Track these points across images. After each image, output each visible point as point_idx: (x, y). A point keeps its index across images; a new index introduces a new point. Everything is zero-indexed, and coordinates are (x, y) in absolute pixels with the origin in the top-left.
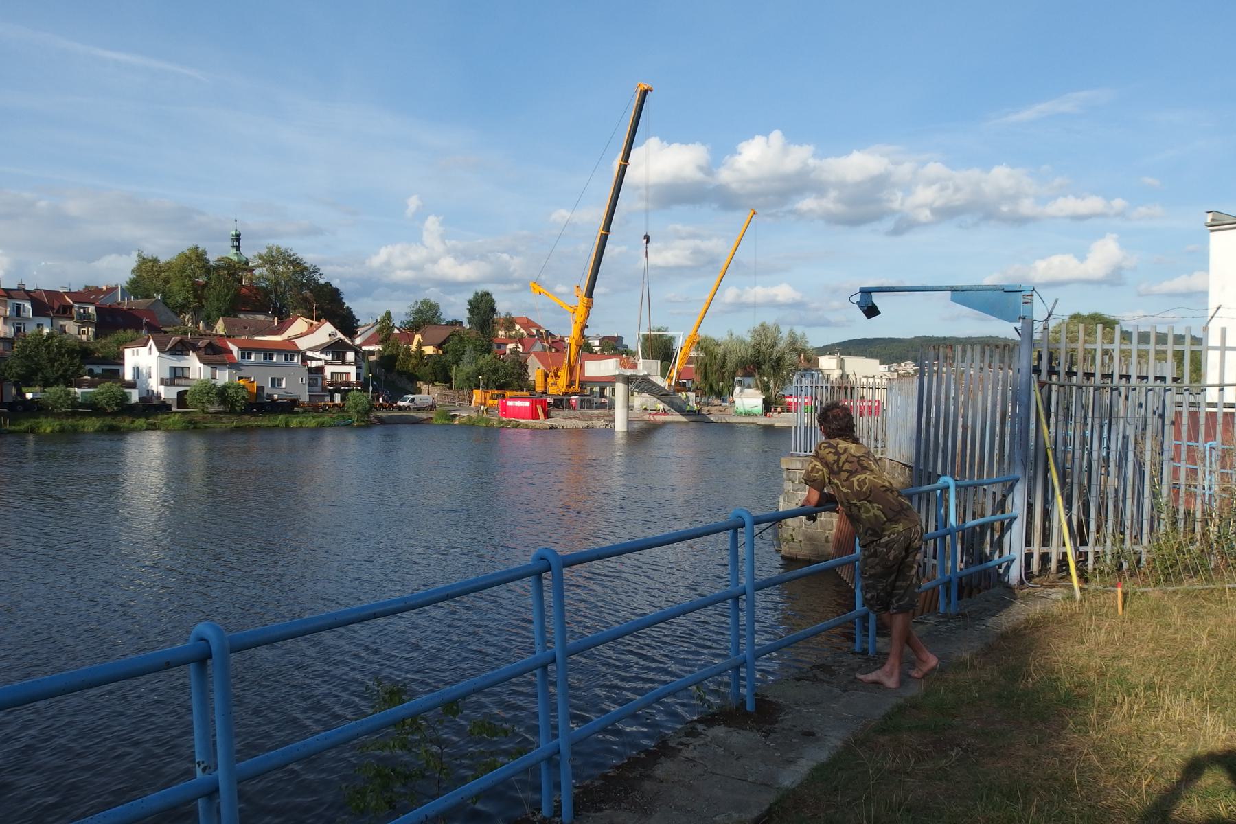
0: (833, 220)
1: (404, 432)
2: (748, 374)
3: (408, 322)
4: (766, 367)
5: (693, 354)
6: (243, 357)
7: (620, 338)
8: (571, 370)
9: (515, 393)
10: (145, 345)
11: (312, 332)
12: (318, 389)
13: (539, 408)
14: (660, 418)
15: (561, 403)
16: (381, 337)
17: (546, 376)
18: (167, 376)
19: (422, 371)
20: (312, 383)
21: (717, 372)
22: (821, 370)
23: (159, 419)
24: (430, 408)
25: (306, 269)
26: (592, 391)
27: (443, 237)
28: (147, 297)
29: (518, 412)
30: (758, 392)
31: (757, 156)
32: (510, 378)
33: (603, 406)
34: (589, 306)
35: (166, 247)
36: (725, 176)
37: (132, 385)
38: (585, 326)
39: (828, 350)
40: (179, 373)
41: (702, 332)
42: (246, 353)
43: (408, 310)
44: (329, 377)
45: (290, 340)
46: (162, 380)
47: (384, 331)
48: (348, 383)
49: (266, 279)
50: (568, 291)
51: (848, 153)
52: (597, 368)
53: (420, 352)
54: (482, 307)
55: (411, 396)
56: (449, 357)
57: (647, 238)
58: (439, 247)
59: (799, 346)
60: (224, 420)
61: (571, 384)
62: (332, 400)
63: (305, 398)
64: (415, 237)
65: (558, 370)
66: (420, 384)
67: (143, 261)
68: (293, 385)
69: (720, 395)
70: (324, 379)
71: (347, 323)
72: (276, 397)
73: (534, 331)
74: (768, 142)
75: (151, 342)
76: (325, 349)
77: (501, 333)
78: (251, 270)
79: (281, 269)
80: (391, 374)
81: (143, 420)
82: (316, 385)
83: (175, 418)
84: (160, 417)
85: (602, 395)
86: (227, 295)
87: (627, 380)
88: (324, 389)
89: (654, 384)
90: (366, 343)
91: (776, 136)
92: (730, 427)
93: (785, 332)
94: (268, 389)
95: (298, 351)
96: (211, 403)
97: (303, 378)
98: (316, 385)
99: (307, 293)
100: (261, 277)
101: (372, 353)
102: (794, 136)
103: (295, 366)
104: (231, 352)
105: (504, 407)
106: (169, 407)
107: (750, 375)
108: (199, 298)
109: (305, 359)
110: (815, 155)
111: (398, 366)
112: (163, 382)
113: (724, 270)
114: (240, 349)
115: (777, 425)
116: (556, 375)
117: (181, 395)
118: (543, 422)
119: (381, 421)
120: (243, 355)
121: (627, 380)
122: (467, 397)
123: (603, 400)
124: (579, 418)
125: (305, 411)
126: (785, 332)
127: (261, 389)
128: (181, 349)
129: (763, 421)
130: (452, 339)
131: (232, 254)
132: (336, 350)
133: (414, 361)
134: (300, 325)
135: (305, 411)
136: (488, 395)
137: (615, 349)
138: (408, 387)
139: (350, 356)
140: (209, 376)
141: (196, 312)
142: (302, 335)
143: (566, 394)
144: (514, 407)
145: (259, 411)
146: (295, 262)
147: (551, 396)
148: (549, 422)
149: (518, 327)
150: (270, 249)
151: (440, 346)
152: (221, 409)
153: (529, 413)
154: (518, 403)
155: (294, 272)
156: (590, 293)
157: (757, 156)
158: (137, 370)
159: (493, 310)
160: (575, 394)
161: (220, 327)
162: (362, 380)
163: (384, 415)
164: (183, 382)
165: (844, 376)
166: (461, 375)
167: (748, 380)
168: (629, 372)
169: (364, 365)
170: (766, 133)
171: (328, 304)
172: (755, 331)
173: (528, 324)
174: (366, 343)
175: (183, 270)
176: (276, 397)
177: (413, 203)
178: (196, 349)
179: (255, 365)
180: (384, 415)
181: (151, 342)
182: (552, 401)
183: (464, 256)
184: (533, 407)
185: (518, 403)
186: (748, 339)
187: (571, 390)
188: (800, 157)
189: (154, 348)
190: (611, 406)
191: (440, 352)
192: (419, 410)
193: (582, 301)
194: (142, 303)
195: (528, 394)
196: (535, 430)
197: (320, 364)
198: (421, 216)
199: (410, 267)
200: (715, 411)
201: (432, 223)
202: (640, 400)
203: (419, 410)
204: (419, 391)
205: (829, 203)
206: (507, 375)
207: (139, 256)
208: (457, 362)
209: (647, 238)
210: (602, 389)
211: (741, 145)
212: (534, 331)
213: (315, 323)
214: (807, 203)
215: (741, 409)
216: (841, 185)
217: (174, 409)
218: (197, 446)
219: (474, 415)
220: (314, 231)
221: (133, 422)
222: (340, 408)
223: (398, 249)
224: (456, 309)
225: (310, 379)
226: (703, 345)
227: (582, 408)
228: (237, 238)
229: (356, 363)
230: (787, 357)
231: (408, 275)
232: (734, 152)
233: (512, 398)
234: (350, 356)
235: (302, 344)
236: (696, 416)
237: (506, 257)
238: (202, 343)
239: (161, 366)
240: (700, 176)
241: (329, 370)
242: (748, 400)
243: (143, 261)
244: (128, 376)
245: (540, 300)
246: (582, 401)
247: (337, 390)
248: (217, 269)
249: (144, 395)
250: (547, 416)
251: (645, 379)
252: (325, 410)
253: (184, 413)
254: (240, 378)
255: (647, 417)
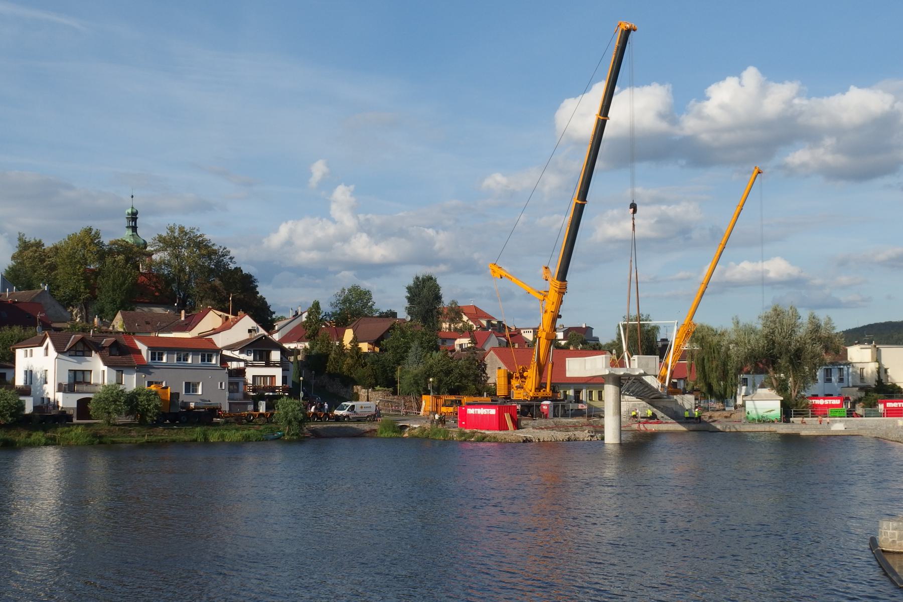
0: (833, 174)
1: (343, 447)
2: (758, 371)
3: (334, 314)
4: (783, 362)
5: (686, 347)
6: (153, 358)
7: (588, 330)
8: (541, 370)
9: (472, 399)
10: (41, 345)
11: (229, 327)
12: (239, 395)
13: (507, 416)
14: (652, 427)
15: (530, 409)
16: (309, 332)
17: (510, 377)
18: (65, 381)
19: (359, 372)
20: (233, 387)
21: (715, 368)
22: (849, 364)
23: (59, 432)
24: (374, 417)
25: (215, 252)
26: (566, 396)
27: (355, 210)
28: (29, 287)
29: (482, 421)
30: (773, 393)
31: (731, 98)
32: (464, 380)
33: (579, 413)
34: (562, 291)
35: (53, 230)
36: (690, 125)
37: (26, 391)
38: (556, 316)
39: (858, 336)
40: (80, 377)
41: (699, 320)
42: (157, 352)
43: (334, 300)
44: (250, 381)
45: (201, 337)
46: (60, 385)
47: (314, 325)
48: (273, 389)
49: (168, 265)
50: (538, 274)
51: (844, 90)
52: (579, 367)
53: (356, 349)
54: (424, 295)
55: (350, 404)
56: (389, 355)
57: (634, 206)
58: (349, 222)
59: (823, 333)
60: (133, 433)
61: (540, 386)
62: (256, 409)
63: (226, 408)
64: (321, 209)
65: (524, 370)
66: (358, 388)
67: (25, 246)
68: (210, 390)
69: (722, 398)
70: (246, 384)
71: (263, 314)
72: (192, 405)
73: (484, 323)
74: (740, 83)
75: (48, 340)
76: (245, 347)
77: (445, 326)
78: (150, 255)
79: (185, 252)
80: (322, 376)
81: (41, 434)
82: (237, 391)
83: (77, 432)
84: (60, 430)
85: (578, 400)
86: (124, 283)
87: (618, 381)
88: (246, 396)
89: (647, 386)
90: (287, 338)
91: (751, 75)
92: (739, 436)
93: (804, 316)
94: (184, 397)
95: (218, 351)
96: (119, 412)
97: (222, 382)
98: (237, 391)
99: (217, 282)
100: (162, 262)
101: (295, 352)
102: (773, 72)
103: (214, 368)
104: (139, 352)
105: (464, 416)
106: (69, 418)
107: (763, 372)
108: (92, 288)
109: (224, 360)
110: (799, 94)
111: (330, 367)
112: (61, 388)
113: (723, 242)
114: (150, 348)
115: (804, 433)
116: (522, 376)
117: (82, 403)
118: (512, 434)
119: (316, 434)
120: (153, 355)
121: (618, 381)
122: (414, 405)
123: (580, 406)
124: (552, 429)
125: (227, 422)
126: (804, 316)
127: (175, 396)
128: (83, 348)
129: (783, 429)
130: (389, 333)
131: (126, 235)
132: (260, 349)
133: (349, 361)
134: (212, 320)
135: (227, 422)
136: (441, 402)
137: (584, 342)
138: (343, 392)
139: (276, 356)
140: (114, 382)
141: (86, 304)
142: (216, 331)
143: (535, 399)
144: (476, 416)
145: (173, 422)
146: (200, 245)
147: (518, 401)
148: (521, 434)
149: (465, 318)
150: (172, 230)
151: (376, 343)
152: (129, 420)
153: (495, 422)
154: (482, 411)
155: (201, 256)
156: (563, 275)
157: (731, 98)
158: (29, 374)
159: (438, 298)
160: (546, 399)
161: (118, 323)
162: (289, 385)
163: (319, 426)
164: (85, 388)
165: (882, 371)
166: (408, 378)
167: (760, 378)
168: (621, 372)
169: (292, 368)
170: (737, 72)
171: (238, 292)
172: (767, 317)
173: (477, 314)
174: (287, 338)
175: (71, 256)
176: (192, 405)
177: (319, 169)
178: (99, 349)
179: (168, 367)
180: (319, 426)
181: (48, 340)
182: (519, 407)
183: (381, 234)
184: (500, 415)
185: (482, 411)
186: (760, 327)
187: (541, 394)
188: (779, 98)
189: (51, 348)
190: (598, 414)
191: (377, 349)
192: (359, 420)
193: (553, 285)
194: (24, 295)
195: (489, 399)
196: (503, 444)
197: (242, 365)
198: (328, 184)
199: (318, 246)
200: (719, 417)
201: (342, 194)
202: (630, 403)
203: (359, 420)
204: (356, 397)
205: (823, 154)
206: (462, 376)
207: (20, 239)
208: (400, 360)
209: (634, 206)
210: (577, 393)
211: (710, 89)
212: (484, 323)
213: (231, 316)
214: (799, 156)
215: (753, 415)
216: (837, 131)
217: (75, 420)
218: (98, 465)
219: (428, 425)
220: (204, 207)
221: (29, 436)
222: (267, 418)
223: (301, 226)
224: (392, 298)
225: (230, 383)
226: (698, 335)
227: (555, 416)
228: (134, 217)
229: (283, 364)
230: (809, 347)
231: (314, 255)
232: (703, 97)
233: (470, 405)
234: (276, 356)
235: (220, 340)
236: (698, 425)
237: (431, 232)
238: (106, 341)
239: (58, 371)
240: (663, 126)
241: (250, 373)
242: (763, 403)
243: (25, 246)
244: (20, 381)
245: (505, 288)
246: (555, 407)
247: (262, 398)
248: (111, 252)
249: (39, 403)
250: (517, 426)
251: (639, 379)
252: (249, 421)
253: (88, 425)
254: (150, 384)
255: (635, 426)
